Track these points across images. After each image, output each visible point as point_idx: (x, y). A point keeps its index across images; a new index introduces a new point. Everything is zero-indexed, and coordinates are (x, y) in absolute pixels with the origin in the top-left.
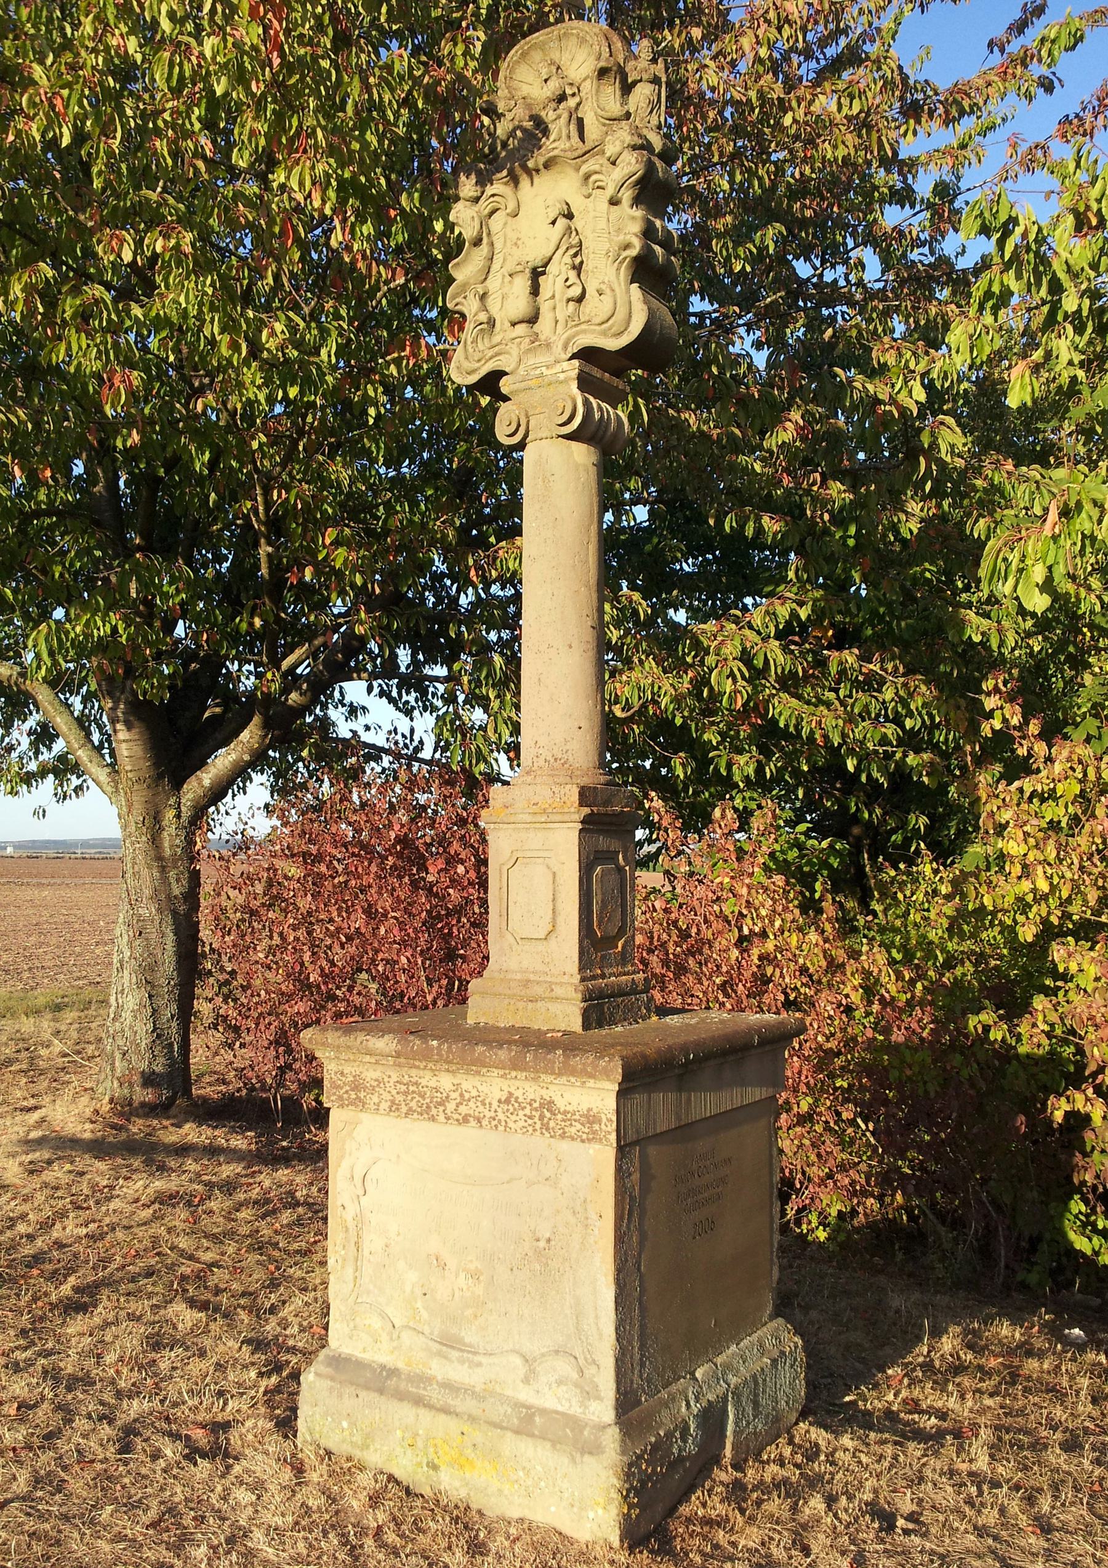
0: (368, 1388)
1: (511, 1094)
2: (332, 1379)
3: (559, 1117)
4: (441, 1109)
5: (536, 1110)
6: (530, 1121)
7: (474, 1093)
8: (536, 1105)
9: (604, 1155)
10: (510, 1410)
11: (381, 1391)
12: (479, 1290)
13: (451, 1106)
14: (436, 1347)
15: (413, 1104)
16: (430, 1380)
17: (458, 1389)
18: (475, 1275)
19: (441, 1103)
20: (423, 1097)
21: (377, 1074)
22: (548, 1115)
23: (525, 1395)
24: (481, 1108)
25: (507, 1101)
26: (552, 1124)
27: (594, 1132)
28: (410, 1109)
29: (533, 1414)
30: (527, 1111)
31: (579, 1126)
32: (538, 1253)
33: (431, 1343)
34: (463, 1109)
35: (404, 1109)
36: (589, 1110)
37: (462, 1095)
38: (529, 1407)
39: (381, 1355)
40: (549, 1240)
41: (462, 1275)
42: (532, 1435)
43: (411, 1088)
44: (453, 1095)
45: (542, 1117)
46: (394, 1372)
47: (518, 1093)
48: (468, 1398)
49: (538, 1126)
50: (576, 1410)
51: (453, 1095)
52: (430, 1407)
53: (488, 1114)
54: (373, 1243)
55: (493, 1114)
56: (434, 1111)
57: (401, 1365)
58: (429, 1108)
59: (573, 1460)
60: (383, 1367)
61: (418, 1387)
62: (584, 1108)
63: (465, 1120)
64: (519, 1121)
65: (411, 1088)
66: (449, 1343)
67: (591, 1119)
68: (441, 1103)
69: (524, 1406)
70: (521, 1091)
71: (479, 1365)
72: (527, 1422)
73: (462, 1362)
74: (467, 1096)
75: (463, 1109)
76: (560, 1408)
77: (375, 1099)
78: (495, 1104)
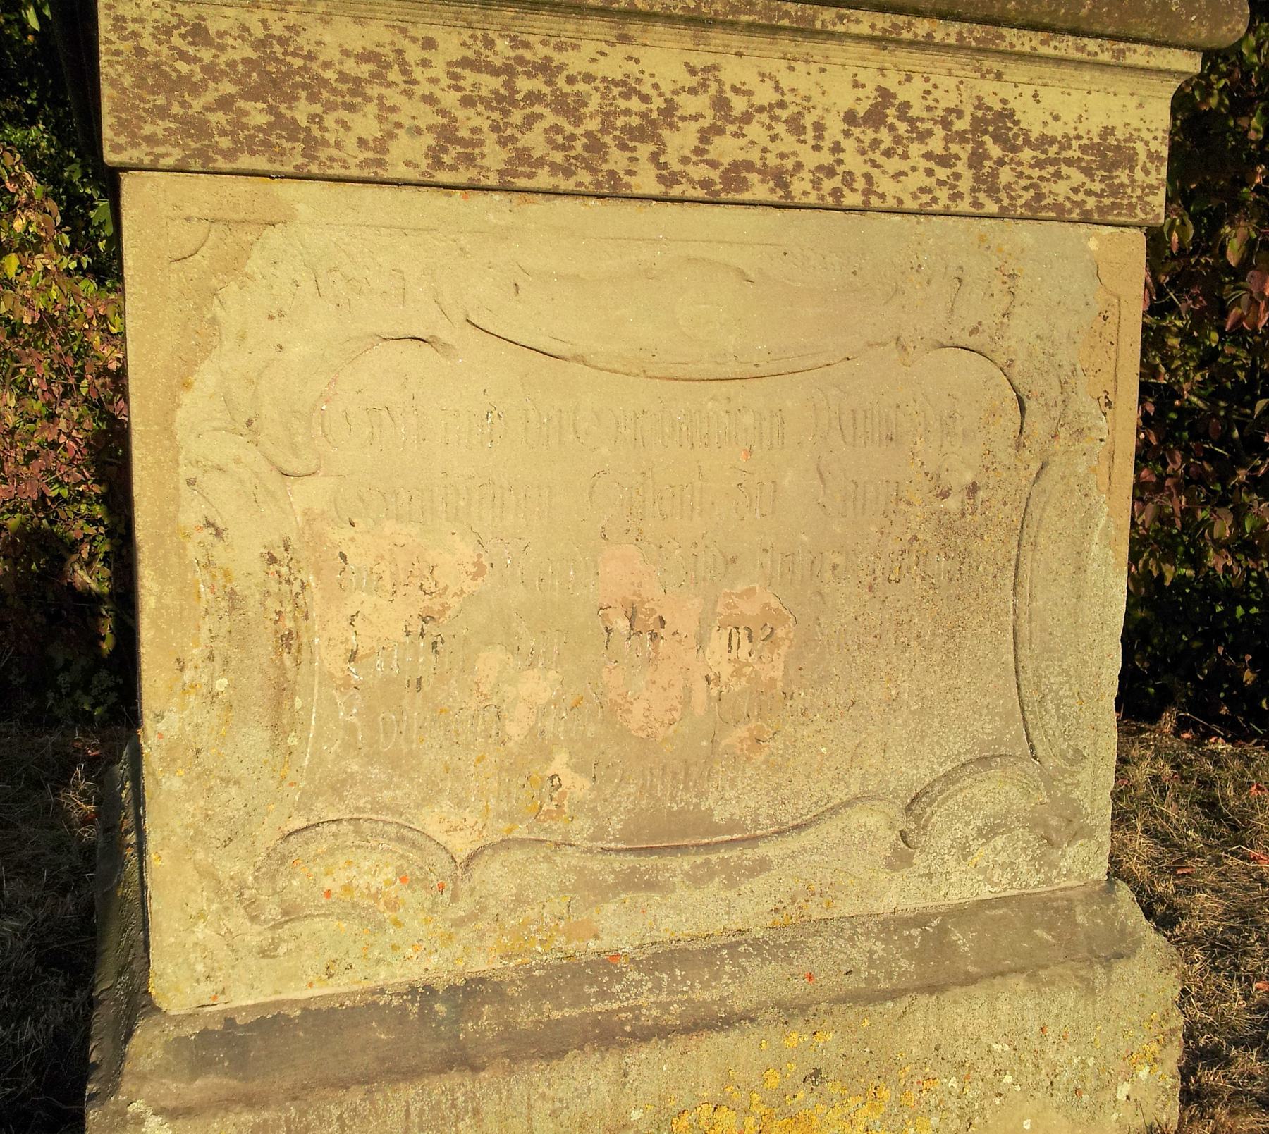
0: (411, 1074)
1: (886, 95)
2: (251, 1102)
3: (1027, 154)
4: (644, 150)
5: (961, 137)
6: (942, 173)
7: (765, 95)
8: (961, 125)
9: (1113, 268)
10: (878, 947)
11: (463, 1060)
12: (774, 669)
13: (680, 141)
14: (606, 868)
15: (534, 140)
16: (607, 964)
17: (711, 952)
18: (761, 632)
19: (647, 131)
20: (570, 109)
21: (376, 35)
22: (995, 151)
23: (898, 895)
24: (788, 143)
25: (875, 118)
26: (1005, 175)
27: (1117, 190)
28: (523, 156)
29: (942, 930)
30: (936, 144)
31: (1077, 177)
32: (947, 527)
33: (596, 864)
34: (726, 148)
35: (494, 157)
36: (1107, 132)
37: (720, 103)
38: (920, 920)
39: (415, 955)
40: (973, 489)
41: (718, 641)
42: (970, 980)
43: (524, 84)
44: (689, 104)
45: (977, 160)
46: (472, 992)
47: (911, 93)
48: (752, 965)
49: (965, 185)
50: (1031, 880)
51: (689, 104)
52: (644, 1035)
53: (811, 160)
54: (360, 623)
55: (826, 158)
56: (617, 160)
57: (480, 965)
58: (595, 164)
59: (1089, 990)
60: (425, 993)
61: (580, 999)
62: (1093, 126)
63: (728, 188)
64: (907, 177)
65: (524, 84)
66: (664, 842)
67: (1109, 155)
68: (647, 131)
69: (907, 923)
70: (918, 84)
71: (763, 866)
72: (937, 955)
73: (697, 879)
74: (739, 105)
75: (726, 148)
76: (986, 892)
77: (366, 124)
78: (835, 127)
